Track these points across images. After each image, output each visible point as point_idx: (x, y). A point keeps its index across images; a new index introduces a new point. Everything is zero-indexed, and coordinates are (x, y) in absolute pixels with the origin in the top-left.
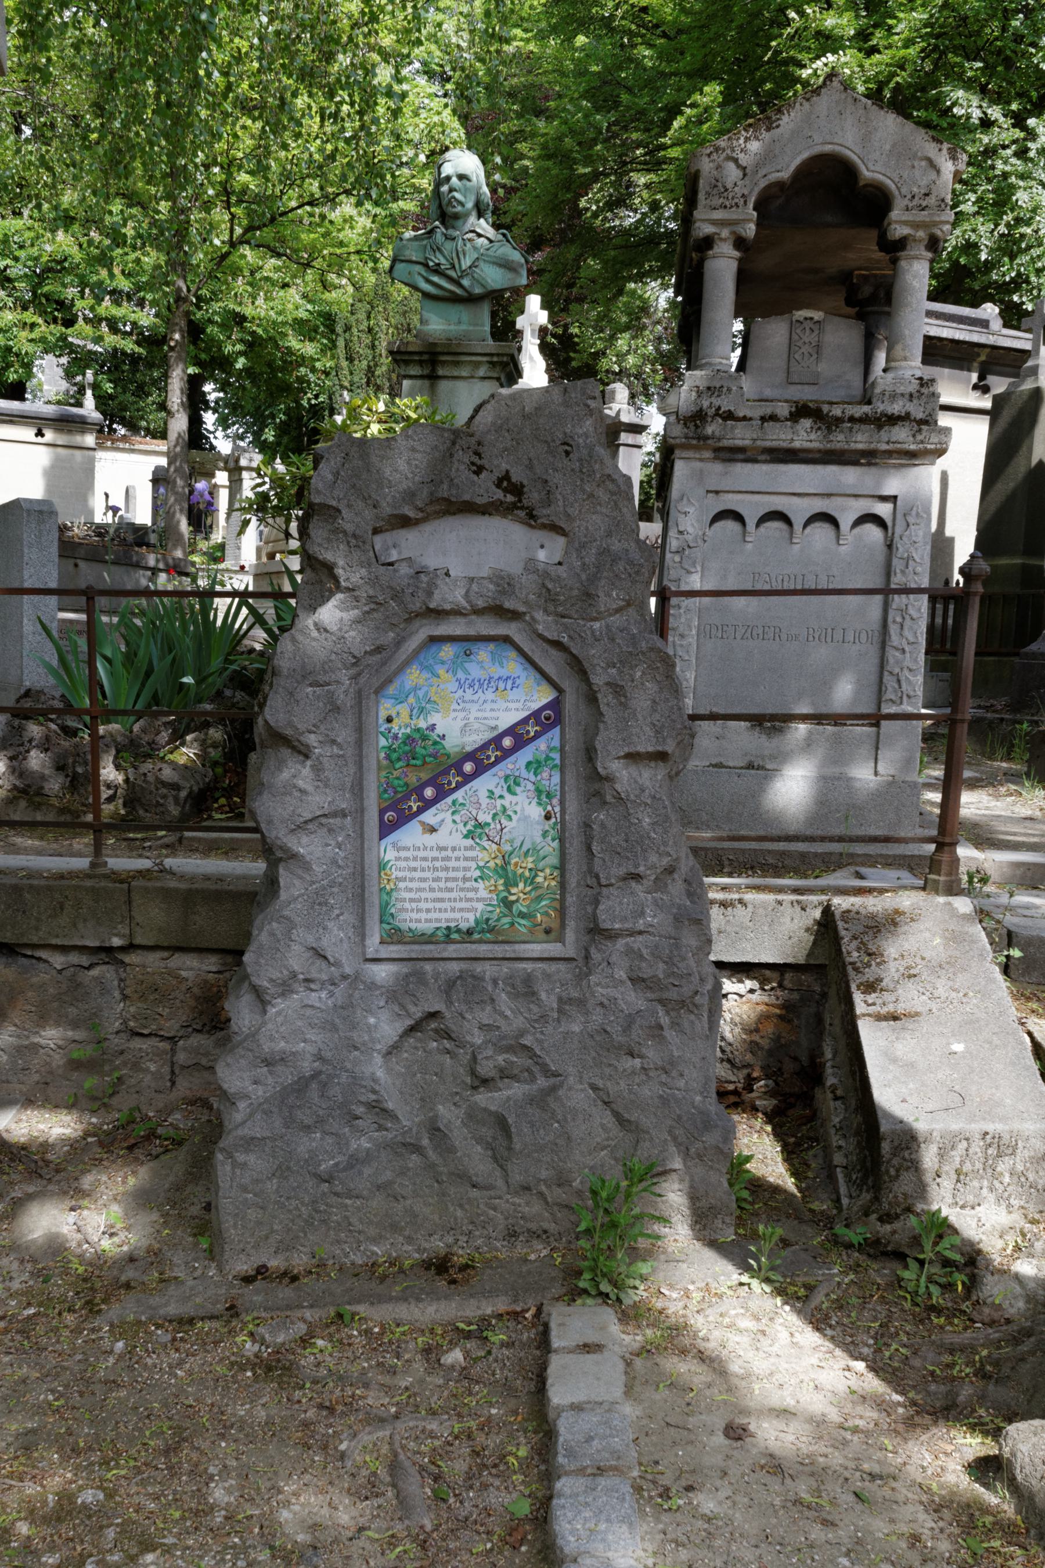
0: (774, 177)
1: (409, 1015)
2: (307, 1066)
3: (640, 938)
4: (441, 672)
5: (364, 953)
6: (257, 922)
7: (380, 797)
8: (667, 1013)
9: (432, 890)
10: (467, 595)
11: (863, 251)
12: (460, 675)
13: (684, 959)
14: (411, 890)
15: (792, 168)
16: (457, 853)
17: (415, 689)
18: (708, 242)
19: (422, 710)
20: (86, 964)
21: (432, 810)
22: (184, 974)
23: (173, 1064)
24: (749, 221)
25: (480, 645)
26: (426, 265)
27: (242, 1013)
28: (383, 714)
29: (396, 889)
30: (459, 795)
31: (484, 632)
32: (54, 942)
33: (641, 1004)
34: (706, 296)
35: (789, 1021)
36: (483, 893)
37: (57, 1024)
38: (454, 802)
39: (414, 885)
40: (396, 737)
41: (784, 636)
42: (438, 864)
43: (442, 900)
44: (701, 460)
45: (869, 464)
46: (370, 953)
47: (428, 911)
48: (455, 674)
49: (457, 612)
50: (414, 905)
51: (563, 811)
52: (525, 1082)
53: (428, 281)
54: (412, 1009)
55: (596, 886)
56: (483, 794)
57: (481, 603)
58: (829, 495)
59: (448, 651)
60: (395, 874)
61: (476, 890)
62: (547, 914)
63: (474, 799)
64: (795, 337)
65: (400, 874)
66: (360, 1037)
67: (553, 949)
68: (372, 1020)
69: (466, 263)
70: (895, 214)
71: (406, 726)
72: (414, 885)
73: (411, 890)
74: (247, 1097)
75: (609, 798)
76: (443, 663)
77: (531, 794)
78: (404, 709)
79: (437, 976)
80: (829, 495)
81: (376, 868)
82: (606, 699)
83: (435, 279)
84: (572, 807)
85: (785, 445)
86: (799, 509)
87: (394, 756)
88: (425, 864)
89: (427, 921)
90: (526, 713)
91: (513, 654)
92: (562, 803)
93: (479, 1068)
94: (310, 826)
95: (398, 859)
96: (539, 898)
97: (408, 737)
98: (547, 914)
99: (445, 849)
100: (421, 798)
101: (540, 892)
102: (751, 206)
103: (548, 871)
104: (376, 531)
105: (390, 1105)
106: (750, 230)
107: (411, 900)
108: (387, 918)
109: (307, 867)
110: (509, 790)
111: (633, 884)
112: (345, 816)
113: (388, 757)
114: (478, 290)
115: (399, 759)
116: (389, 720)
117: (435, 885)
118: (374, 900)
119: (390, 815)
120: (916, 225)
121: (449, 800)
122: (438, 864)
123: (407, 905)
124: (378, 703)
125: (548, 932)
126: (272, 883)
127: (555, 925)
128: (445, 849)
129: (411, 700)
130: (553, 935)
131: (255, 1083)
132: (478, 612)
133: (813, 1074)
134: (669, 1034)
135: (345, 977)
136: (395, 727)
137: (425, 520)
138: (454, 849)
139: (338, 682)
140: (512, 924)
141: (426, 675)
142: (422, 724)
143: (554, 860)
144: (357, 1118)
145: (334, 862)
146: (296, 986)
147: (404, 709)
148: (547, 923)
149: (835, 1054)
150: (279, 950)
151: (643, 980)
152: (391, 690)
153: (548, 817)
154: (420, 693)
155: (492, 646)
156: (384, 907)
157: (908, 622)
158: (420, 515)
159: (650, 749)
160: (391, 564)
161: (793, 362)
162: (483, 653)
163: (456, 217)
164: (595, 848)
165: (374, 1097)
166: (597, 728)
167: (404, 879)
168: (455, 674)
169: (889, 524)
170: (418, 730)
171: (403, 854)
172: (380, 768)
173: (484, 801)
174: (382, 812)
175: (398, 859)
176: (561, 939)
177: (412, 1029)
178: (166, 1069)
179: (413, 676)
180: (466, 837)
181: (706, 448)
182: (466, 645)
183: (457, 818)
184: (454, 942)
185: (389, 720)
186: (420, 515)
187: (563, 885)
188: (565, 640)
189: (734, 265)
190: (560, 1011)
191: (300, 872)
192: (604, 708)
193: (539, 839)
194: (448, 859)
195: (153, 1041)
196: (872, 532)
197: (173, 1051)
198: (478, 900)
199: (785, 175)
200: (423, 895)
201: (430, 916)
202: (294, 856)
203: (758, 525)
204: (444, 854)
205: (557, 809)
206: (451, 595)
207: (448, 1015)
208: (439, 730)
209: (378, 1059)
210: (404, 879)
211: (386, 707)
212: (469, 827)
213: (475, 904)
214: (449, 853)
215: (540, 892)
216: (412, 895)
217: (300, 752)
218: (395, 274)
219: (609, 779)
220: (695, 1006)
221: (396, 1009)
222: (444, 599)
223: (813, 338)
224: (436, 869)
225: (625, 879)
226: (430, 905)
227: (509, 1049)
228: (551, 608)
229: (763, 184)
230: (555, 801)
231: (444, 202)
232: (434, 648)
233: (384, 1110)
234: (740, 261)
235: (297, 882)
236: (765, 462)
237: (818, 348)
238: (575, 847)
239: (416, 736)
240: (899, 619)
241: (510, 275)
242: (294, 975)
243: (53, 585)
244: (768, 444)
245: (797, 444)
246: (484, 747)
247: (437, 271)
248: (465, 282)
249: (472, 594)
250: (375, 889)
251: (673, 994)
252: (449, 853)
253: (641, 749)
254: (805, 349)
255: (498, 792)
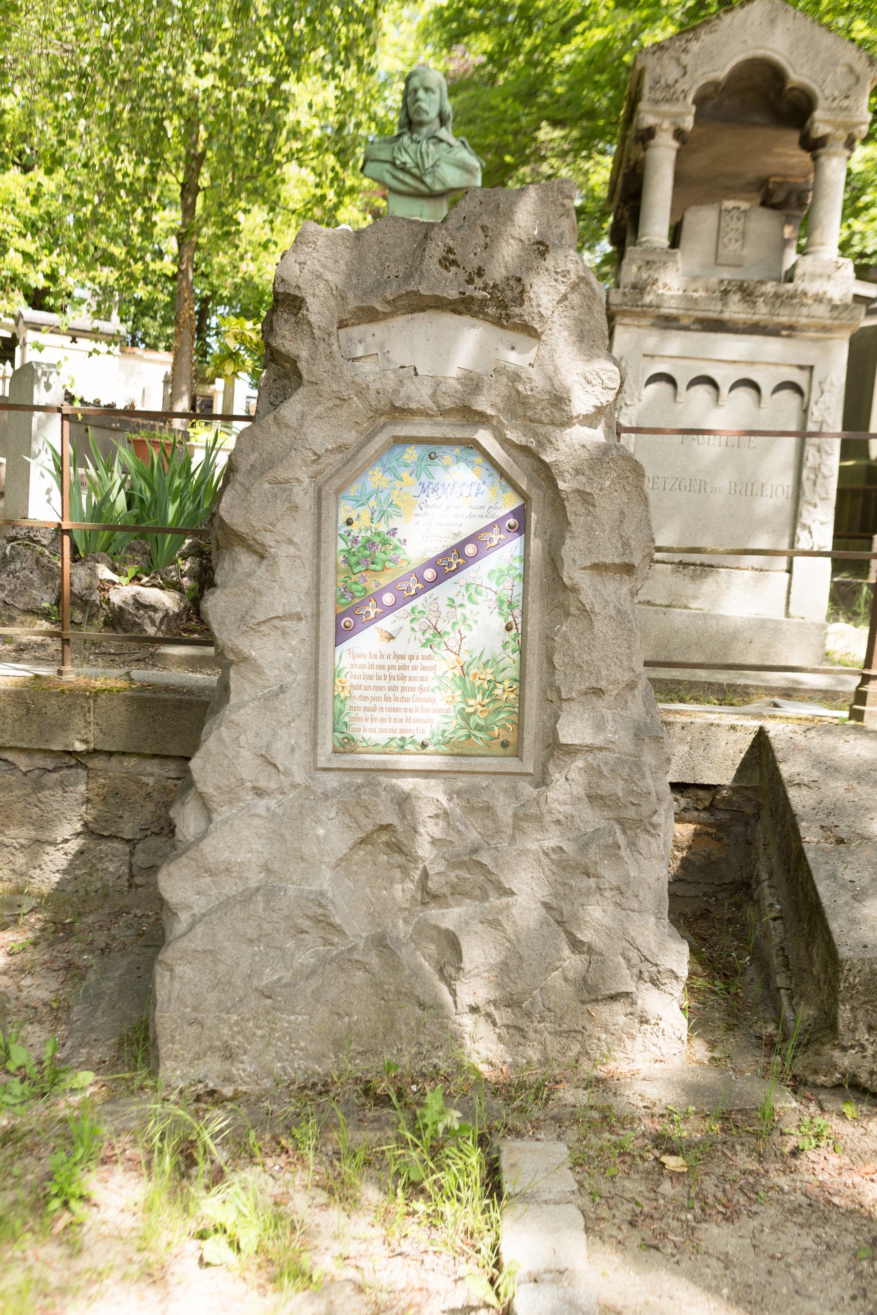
0: (712, 76)
1: (360, 827)
2: (255, 879)
3: (600, 755)
4: (405, 474)
5: (315, 762)
6: (207, 727)
7: (337, 602)
8: (624, 832)
9: (387, 699)
10: (434, 395)
11: (785, 155)
12: (424, 478)
13: (643, 776)
14: (366, 698)
15: (728, 69)
16: (414, 662)
17: (377, 491)
18: (649, 133)
19: (383, 513)
20: (50, 767)
21: (391, 617)
22: (145, 779)
23: (131, 866)
24: (689, 113)
25: (444, 448)
26: (393, 164)
27: (188, 820)
28: (343, 517)
29: (351, 697)
30: (418, 602)
31: (450, 435)
32: (19, 745)
33: (603, 823)
34: (646, 181)
35: (720, 840)
36: (441, 704)
37: (21, 824)
38: (413, 610)
39: (370, 693)
40: (355, 540)
41: (708, 489)
42: (394, 673)
43: (397, 710)
44: (639, 327)
45: (789, 336)
46: (322, 762)
47: (383, 720)
48: (418, 477)
49: (423, 413)
50: (368, 714)
51: (525, 622)
52: (475, 898)
53: (395, 177)
54: (363, 821)
55: (554, 701)
56: (443, 603)
57: (448, 403)
58: (753, 363)
59: (412, 453)
60: (350, 682)
61: (433, 701)
62: (504, 727)
63: (434, 607)
64: (723, 224)
65: (355, 682)
66: (309, 849)
67: (511, 765)
68: (321, 832)
69: (428, 163)
70: (818, 114)
71: (367, 529)
72: (370, 693)
73: (366, 698)
74: (189, 907)
75: (573, 610)
76: (406, 465)
77: (493, 604)
78: (365, 512)
79: (392, 789)
80: (753, 363)
81: (330, 674)
82: (573, 507)
83: (401, 175)
84: (534, 619)
85: (715, 315)
86: (724, 376)
87: (353, 560)
88: (381, 672)
89: (381, 731)
90: (492, 520)
91: (479, 459)
92: (524, 613)
93: (430, 884)
94: (263, 628)
95: (353, 666)
96: (498, 711)
97: (369, 540)
98: (504, 727)
99: (403, 657)
100: (379, 604)
101: (498, 704)
102: (690, 100)
103: (507, 684)
104: (342, 325)
105: (337, 920)
106: (688, 123)
107: (366, 709)
108: (338, 727)
109: (258, 670)
110: (470, 598)
111: (594, 699)
112: (300, 619)
113: (346, 561)
114: (438, 187)
115: (358, 563)
116: (349, 522)
117: (390, 694)
118: (326, 697)
119: (347, 620)
120: (838, 126)
121: (408, 607)
122: (394, 673)
123: (361, 714)
124: (337, 503)
125: (505, 745)
126: (224, 688)
127: (512, 739)
128: (403, 657)
129: (373, 502)
130: (510, 750)
131: (198, 893)
132: (444, 412)
133: (744, 888)
134: (624, 853)
135: (294, 786)
136: (355, 529)
137: (393, 314)
138: (411, 658)
139: (298, 480)
140: (469, 737)
141: (389, 477)
142: (383, 528)
143: (514, 672)
144: (303, 932)
145: (288, 667)
146: (243, 793)
147: (365, 512)
148: (505, 736)
149: (771, 874)
150: (226, 754)
151: (602, 798)
152: (352, 491)
153: (508, 628)
154: (382, 496)
155: (457, 450)
156: (337, 716)
157: (820, 480)
158: (387, 309)
159: (617, 561)
160: (354, 359)
161: (721, 246)
162: (448, 455)
163: (421, 124)
164: (557, 659)
165: (321, 911)
166: (563, 537)
167: (359, 687)
168: (418, 477)
169: (805, 389)
170: (378, 534)
171: (359, 661)
172: (337, 571)
173: (444, 609)
174: (339, 617)
175: (353, 666)
176: (518, 754)
177: (363, 841)
178: (125, 869)
179: (375, 478)
180: (424, 645)
181: (644, 315)
182: (432, 448)
183: (415, 625)
184: (408, 753)
185: (349, 522)
186: (387, 309)
187: (521, 698)
188: (533, 445)
189: (672, 155)
190: (515, 827)
191: (251, 676)
192: (571, 517)
193: (499, 650)
194: (405, 667)
195: (117, 845)
196: (788, 397)
197: (132, 854)
198: (435, 711)
199: (721, 74)
200: (379, 704)
201: (385, 726)
202: (245, 659)
203: (688, 387)
204: (401, 662)
205: (519, 620)
206: (420, 394)
207: (400, 829)
208: (400, 535)
209: (327, 873)
210: (359, 687)
211: (346, 510)
212: (428, 635)
213: (431, 715)
214: (406, 662)
215: (498, 704)
216: (367, 704)
217: (255, 552)
218: (366, 171)
219: (575, 590)
220: (653, 826)
221: (347, 820)
222: (409, 398)
223: (740, 225)
224: (392, 678)
225: (586, 694)
226: (385, 715)
227: (461, 865)
228: (520, 411)
229: (701, 83)
230: (517, 612)
231: (411, 112)
232: (398, 450)
233: (330, 924)
234: (679, 151)
235: (248, 686)
236: (697, 330)
237: (744, 234)
238: (534, 662)
239: (377, 540)
240: (812, 477)
241: (467, 176)
242: (242, 782)
243: (37, 415)
244: (700, 314)
245: (726, 316)
246: (446, 554)
247: (403, 169)
248: (428, 180)
249: (439, 393)
250: (329, 696)
251: (631, 813)
252: (406, 662)
253: (608, 561)
254: (732, 235)
255: (458, 601)
